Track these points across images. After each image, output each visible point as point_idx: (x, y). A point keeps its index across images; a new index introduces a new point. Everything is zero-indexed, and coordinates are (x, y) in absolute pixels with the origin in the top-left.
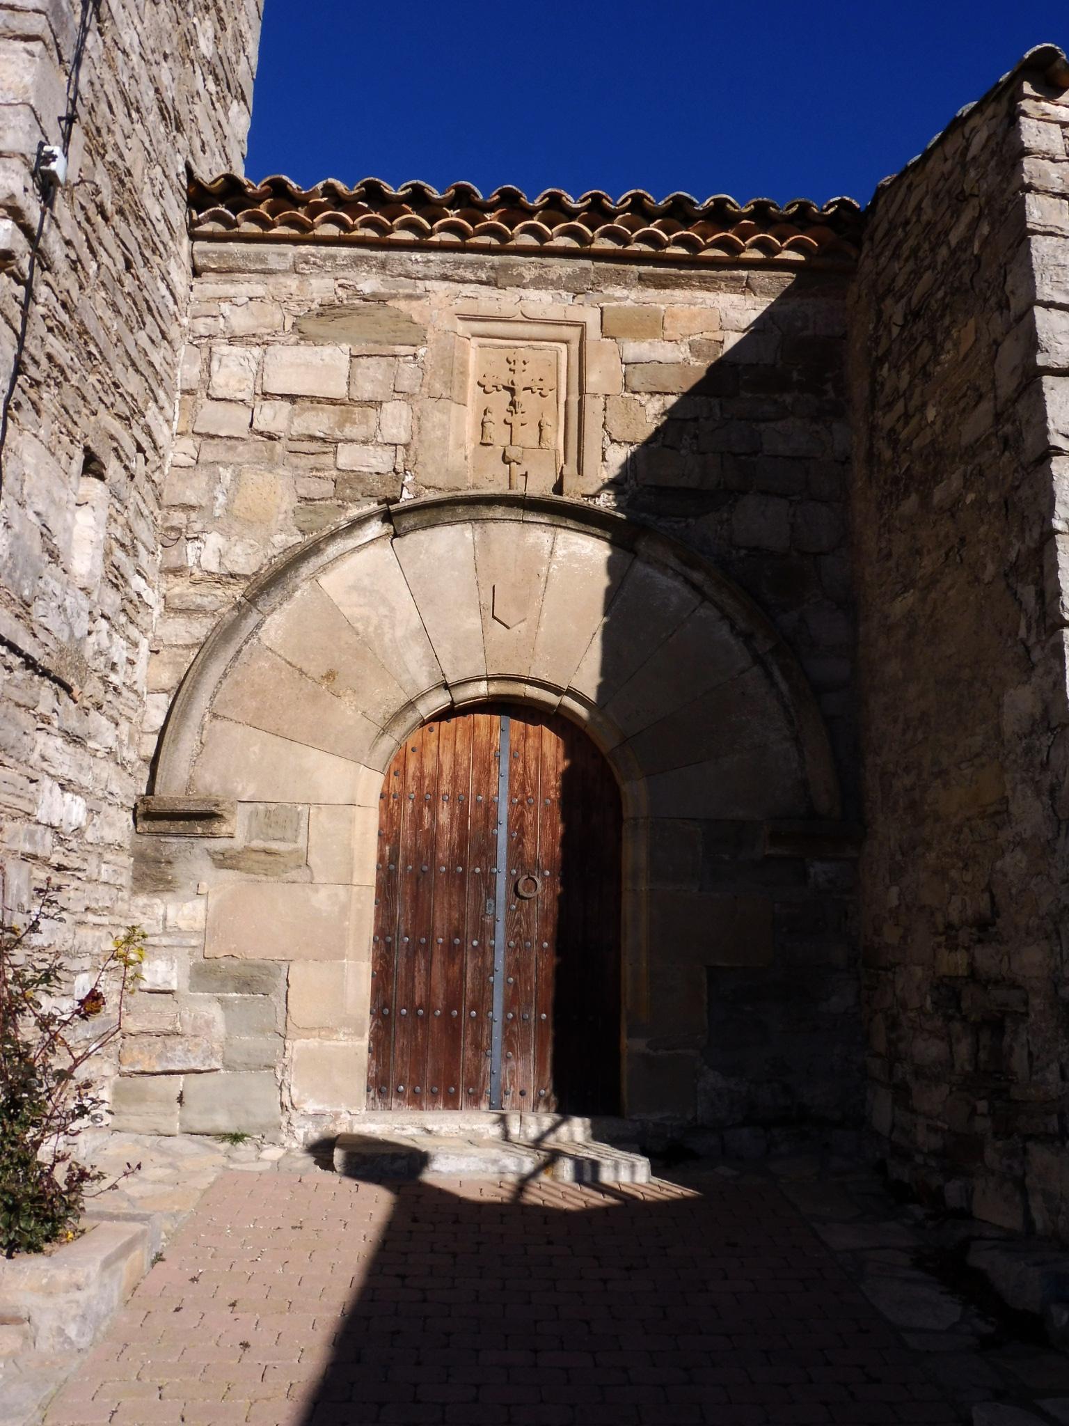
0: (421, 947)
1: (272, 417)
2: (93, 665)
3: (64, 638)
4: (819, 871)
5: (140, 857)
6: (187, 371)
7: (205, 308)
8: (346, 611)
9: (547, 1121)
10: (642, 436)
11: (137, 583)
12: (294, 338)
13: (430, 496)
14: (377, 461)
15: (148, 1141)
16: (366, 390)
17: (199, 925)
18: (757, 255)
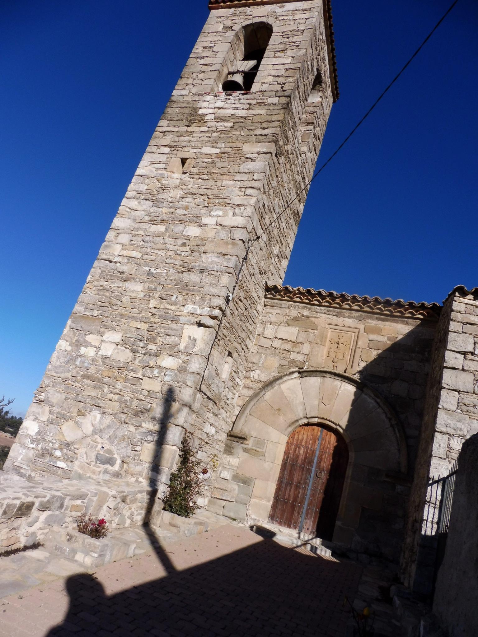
0: (289, 483)
1: (277, 343)
2: (223, 398)
3: (217, 392)
4: (399, 488)
5: (227, 445)
6: (259, 330)
7: (266, 315)
8: (285, 394)
9: (311, 537)
10: (370, 361)
11: (238, 380)
12: (285, 325)
13: (311, 369)
14: (300, 358)
15: (214, 515)
16: (300, 340)
17: (237, 465)
18: (410, 315)
